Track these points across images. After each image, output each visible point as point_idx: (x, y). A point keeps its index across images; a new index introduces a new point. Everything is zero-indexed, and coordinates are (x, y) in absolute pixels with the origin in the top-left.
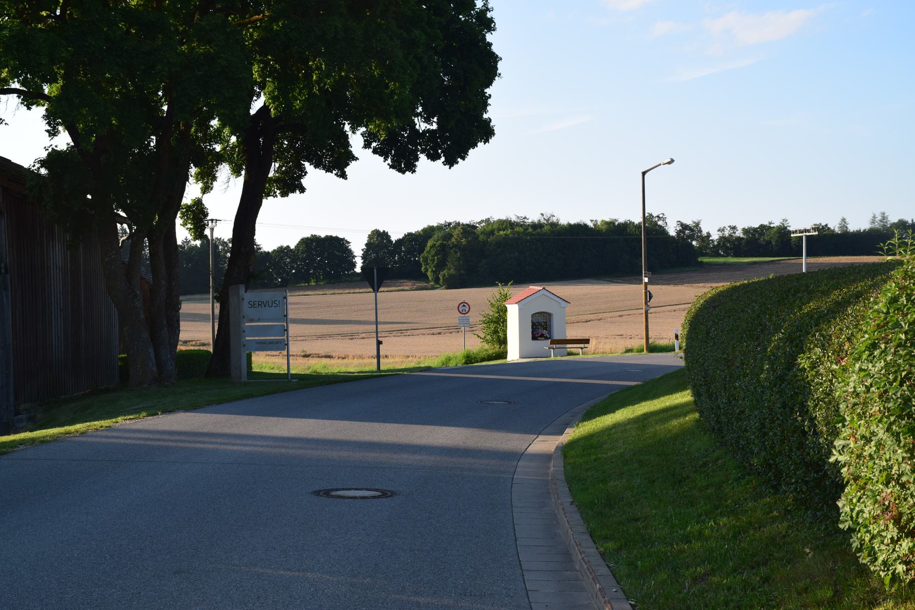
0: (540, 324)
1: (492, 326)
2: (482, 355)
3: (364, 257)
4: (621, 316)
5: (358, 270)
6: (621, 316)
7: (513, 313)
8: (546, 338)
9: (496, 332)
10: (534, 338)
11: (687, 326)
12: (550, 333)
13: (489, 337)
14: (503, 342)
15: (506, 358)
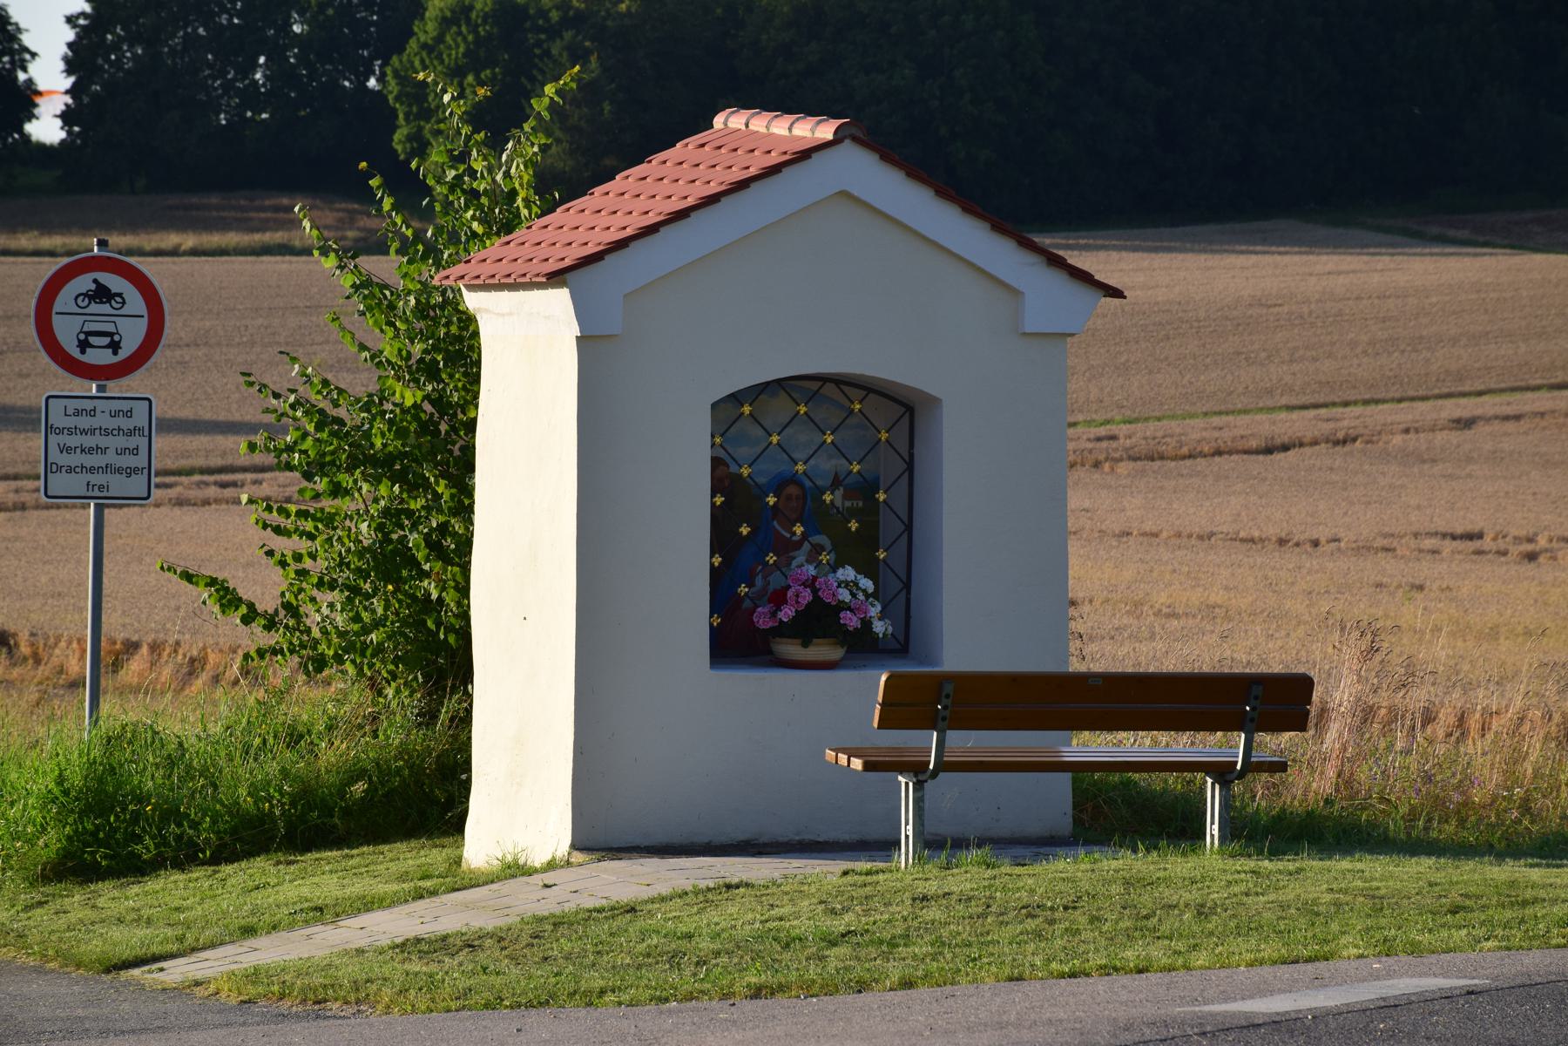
0: (800, 498)
1: (363, 504)
2: (246, 782)
3: (78, 60)
4: (1466, 423)
5: (46, 128)
6: (1466, 423)
7: (528, 352)
8: (862, 647)
9: (389, 562)
10: (738, 640)
11: (15, 232)
12: (903, 588)
13: (325, 611)
14: (443, 661)
15: (456, 826)
